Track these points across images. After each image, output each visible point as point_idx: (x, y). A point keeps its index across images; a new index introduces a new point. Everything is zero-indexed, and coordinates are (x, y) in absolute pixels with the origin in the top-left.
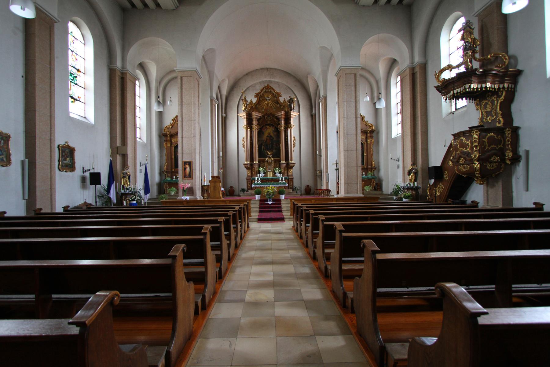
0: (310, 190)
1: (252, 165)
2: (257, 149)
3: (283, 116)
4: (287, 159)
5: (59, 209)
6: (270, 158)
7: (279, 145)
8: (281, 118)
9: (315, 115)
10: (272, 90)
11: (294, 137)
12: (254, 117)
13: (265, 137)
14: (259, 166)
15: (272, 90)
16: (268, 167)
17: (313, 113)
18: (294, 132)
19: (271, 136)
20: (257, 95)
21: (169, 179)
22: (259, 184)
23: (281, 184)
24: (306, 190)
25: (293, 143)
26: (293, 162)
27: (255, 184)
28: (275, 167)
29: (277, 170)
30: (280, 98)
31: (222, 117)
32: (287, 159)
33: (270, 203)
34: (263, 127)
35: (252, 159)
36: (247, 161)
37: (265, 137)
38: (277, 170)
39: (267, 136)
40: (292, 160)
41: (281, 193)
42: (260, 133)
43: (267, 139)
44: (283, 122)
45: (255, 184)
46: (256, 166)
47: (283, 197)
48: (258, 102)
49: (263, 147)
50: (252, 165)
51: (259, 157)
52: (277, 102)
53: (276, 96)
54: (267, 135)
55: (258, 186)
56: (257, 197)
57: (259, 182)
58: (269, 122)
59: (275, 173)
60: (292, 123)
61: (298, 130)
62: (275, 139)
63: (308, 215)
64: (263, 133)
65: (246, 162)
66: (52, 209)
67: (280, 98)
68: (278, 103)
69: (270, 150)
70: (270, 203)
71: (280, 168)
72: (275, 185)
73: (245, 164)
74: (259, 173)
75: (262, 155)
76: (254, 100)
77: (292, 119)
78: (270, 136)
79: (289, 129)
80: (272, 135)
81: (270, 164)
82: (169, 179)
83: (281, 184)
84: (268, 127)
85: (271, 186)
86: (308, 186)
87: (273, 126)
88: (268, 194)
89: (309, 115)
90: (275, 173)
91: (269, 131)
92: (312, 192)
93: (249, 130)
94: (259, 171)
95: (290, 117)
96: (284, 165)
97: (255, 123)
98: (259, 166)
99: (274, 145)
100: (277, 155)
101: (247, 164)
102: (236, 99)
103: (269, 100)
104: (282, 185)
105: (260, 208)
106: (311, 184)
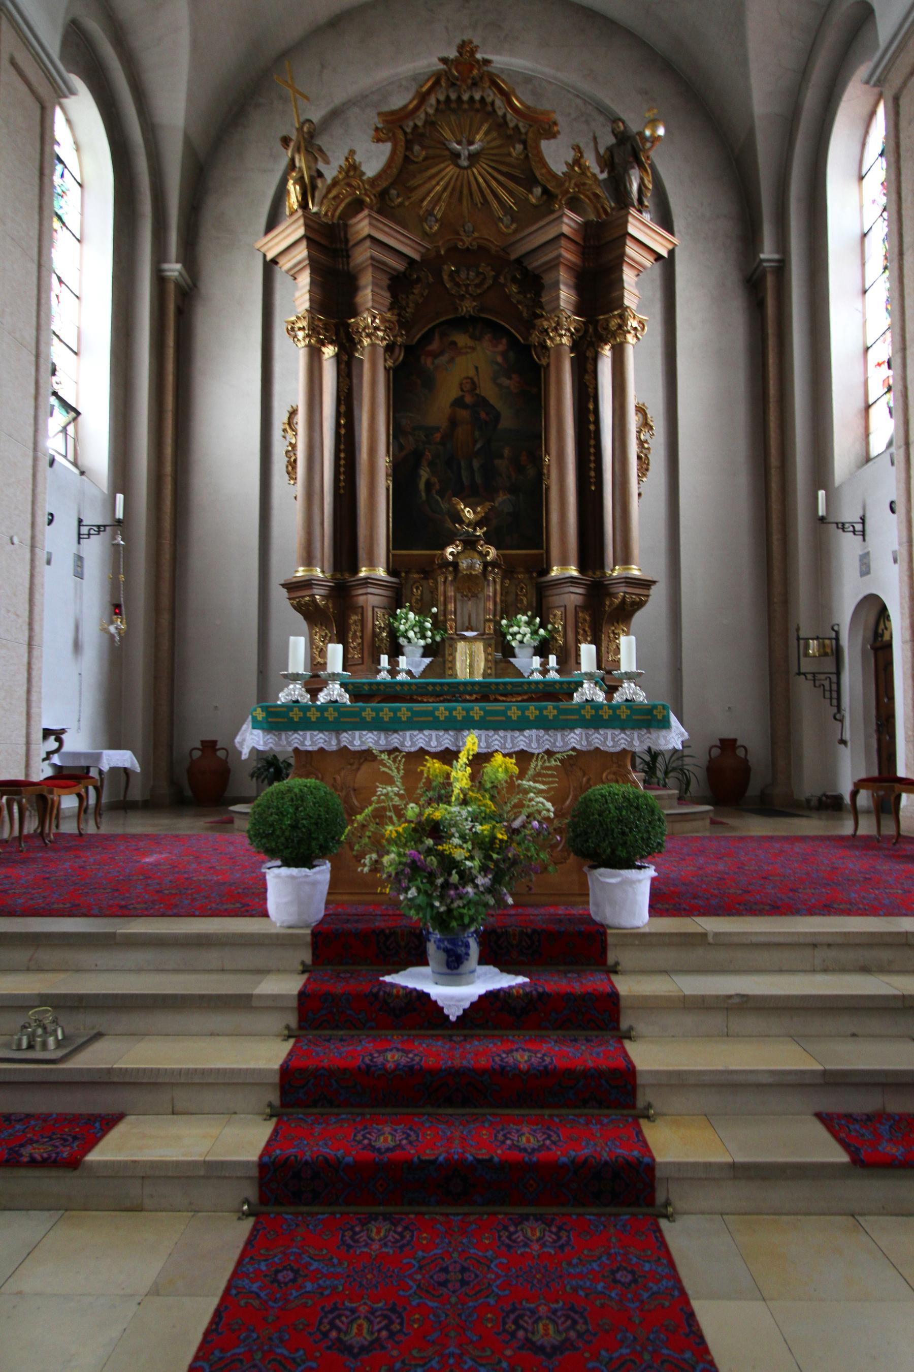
0: (744, 770)
1: (343, 590)
2: (383, 483)
3: (568, 254)
4: (590, 552)
5: (578, 731)
6: (470, 544)
7: (537, 460)
8: (554, 264)
9: (782, 268)
10: (491, 95)
11: (641, 410)
12: (362, 255)
13: (440, 405)
14: (396, 599)
15: (491, 95)
16: (459, 609)
17: (768, 253)
18: (635, 370)
19: (482, 402)
20: (392, 126)
22: (334, 720)
23: (594, 717)
24: (713, 770)
25: (633, 449)
26: (635, 571)
27: (279, 720)
28: (509, 610)
29: (521, 631)
30: (547, 147)
31: (160, 280)
32: (590, 552)
33: (455, 994)
34: (427, 338)
35: (346, 550)
36: (309, 561)
37: (440, 405)
38: (521, 631)
39: (458, 403)
40: (626, 559)
41: (604, 837)
42: (408, 381)
43: (453, 422)
44: (566, 296)
45: (279, 720)
46: (371, 600)
47: (629, 897)
48: (401, 175)
49: (424, 474)
50: (343, 590)
51: (398, 539)
52: (528, 173)
53: (515, 136)
54: (455, 393)
55: (313, 741)
56: (290, 895)
57: (334, 692)
58: (467, 307)
59: (503, 649)
60: (630, 300)
61: (661, 380)
62: (507, 421)
64: (429, 383)
65: (301, 572)
66: (27, 775)
67: (547, 147)
68: (530, 181)
69: (472, 496)
70: (455, 994)
71: (541, 610)
72: (530, 740)
73: (292, 587)
74: (396, 651)
75: (416, 526)
76: (374, 159)
77: (628, 276)
78: (473, 404)
79: (607, 351)
80: (488, 390)
81: (469, 586)
83: (594, 717)
84: (462, 340)
85: (472, 742)
86: (728, 745)
87: (497, 331)
88: (432, 866)
89: (733, 278)
90: (509, 652)
91: (470, 367)
92: (753, 789)
93: (329, 351)
94: (394, 634)
95: (620, 259)
96: (573, 597)
97: (371, 314)
98: (396, 599)
99: (501, 464)
100: (521, 529)
101: (307, 584)
102: (263, 172)
103: (473, 157)
104: (611, 740)
105: (298, 1091)
106: (750, 734)
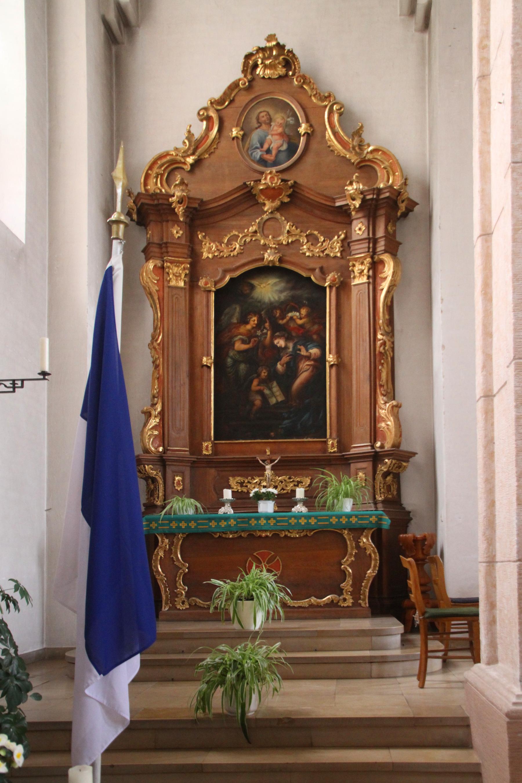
21: (186, 507)
63: (262, 173)
82: (186, 507)
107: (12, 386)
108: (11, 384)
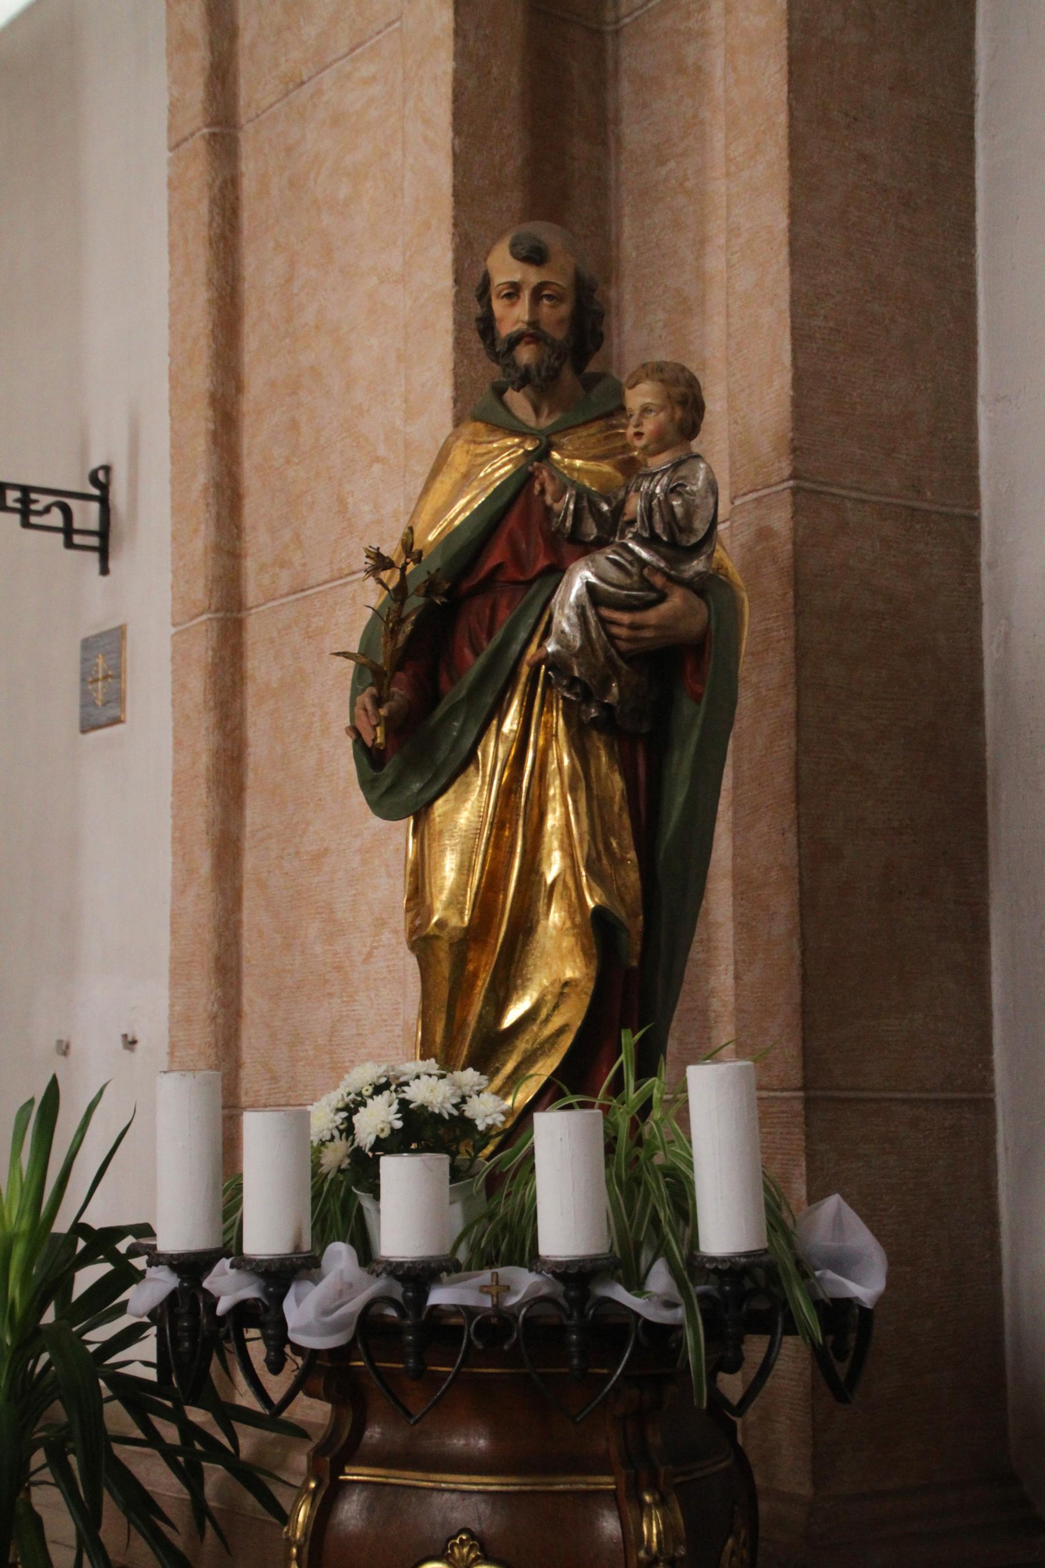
107: (18, 505)
108: (36, 501)
